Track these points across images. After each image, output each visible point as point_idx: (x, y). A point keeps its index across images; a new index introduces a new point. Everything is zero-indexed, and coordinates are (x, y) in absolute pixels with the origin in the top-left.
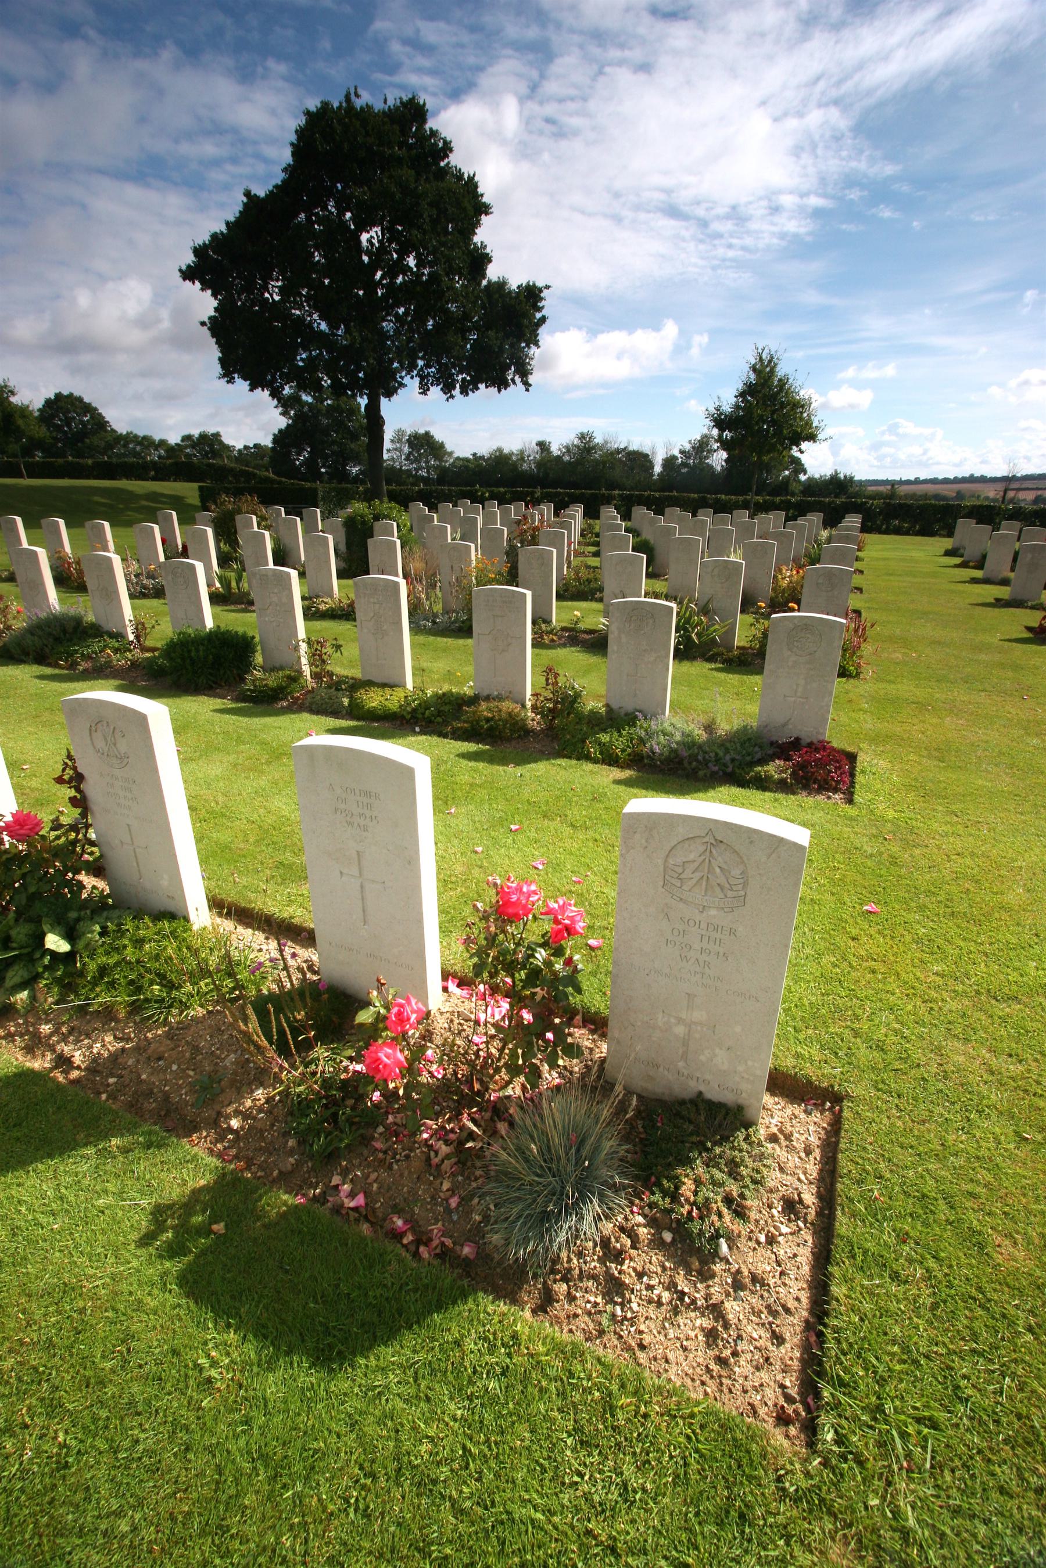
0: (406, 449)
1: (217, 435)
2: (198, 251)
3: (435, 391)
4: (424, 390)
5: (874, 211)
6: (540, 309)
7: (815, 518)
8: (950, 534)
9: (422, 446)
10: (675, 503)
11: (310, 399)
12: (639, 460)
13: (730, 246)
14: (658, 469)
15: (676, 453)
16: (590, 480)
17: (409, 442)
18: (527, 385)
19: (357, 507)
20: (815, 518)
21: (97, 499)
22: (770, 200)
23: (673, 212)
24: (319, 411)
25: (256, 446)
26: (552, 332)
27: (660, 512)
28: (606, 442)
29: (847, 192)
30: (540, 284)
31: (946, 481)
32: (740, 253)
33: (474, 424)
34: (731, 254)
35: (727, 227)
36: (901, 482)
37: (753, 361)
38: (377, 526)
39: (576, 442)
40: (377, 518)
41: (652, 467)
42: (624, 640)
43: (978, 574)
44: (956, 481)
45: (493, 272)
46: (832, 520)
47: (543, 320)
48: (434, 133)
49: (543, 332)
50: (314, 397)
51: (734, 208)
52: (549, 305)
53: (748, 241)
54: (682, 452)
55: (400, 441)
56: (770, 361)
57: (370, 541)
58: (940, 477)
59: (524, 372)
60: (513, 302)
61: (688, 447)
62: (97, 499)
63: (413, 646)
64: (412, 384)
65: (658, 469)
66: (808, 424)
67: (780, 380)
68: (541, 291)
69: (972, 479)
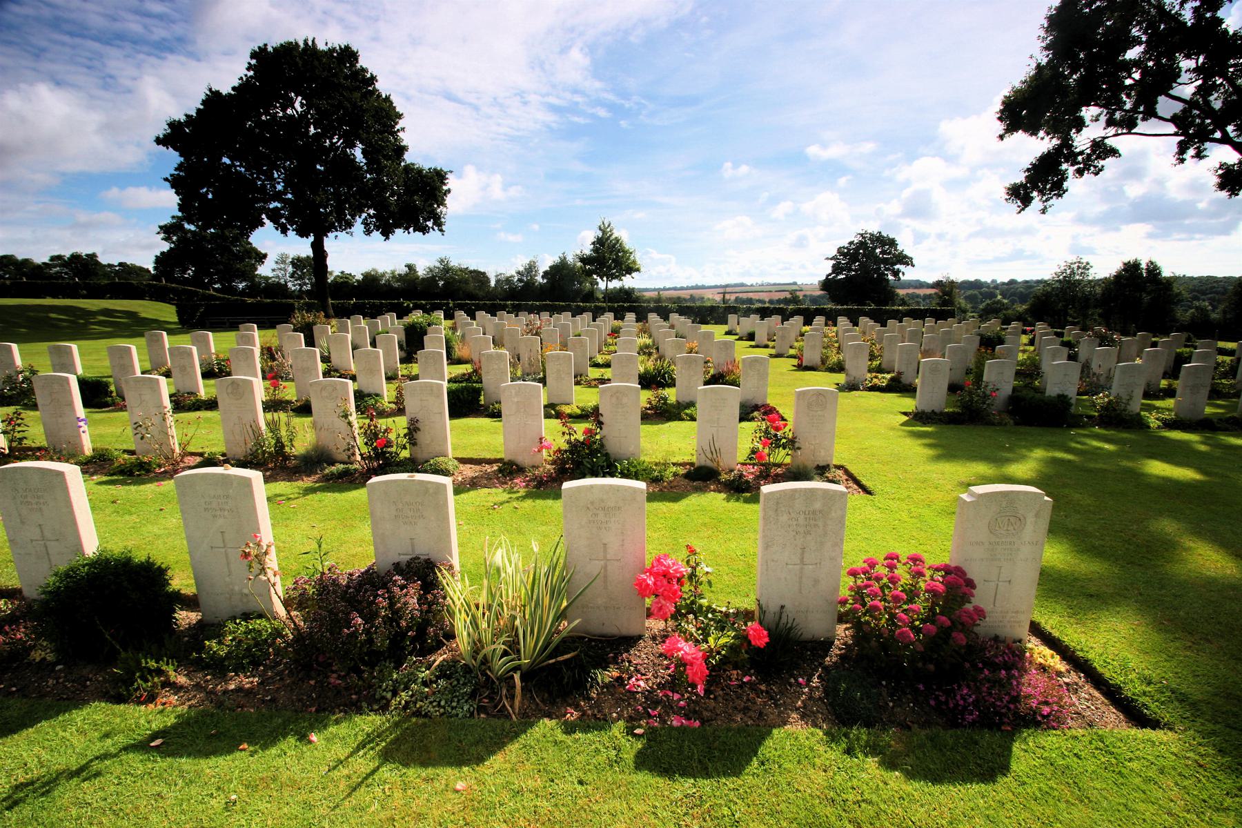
0: (290, 269)
1: (92, 257)
2: (172, 125)
3: (376, 235)
4: (368, 232)
7: (798, 319)
8: (726, 323)
9: (305, 267)
10: (503, 308)
11: (192, 228)
12: (480, 277)
14: (493, 283)
16: (457, 292)
17: (292, 263)
18: (441, 230)
19: (417, 316)
20: (798, 319)
21: (53, 315)
23: (450, 97)
24: (205, 237)
25: (121, 264)
27: (494, 315)
31: (682, 289)
33: (356, 253)
34: (502, 130)
36: (664, 289)
38: (429, 329)
39: (438, 265)
40: (429, 325)
43: (753, 343)
44: (688, 288)
45: (409, 158)
46: (619, 316)
47: (449, 191)
48: (364, 70)
50: (197, 226)
54: (519, 273)
55: (284, 262)
57: (425, 338)
59: (439, 223)
61: (521, 269)
62: (53, 315)
64: (358, 227)
65: (493, 283)
66: (634, 262)
69: (697, 287)
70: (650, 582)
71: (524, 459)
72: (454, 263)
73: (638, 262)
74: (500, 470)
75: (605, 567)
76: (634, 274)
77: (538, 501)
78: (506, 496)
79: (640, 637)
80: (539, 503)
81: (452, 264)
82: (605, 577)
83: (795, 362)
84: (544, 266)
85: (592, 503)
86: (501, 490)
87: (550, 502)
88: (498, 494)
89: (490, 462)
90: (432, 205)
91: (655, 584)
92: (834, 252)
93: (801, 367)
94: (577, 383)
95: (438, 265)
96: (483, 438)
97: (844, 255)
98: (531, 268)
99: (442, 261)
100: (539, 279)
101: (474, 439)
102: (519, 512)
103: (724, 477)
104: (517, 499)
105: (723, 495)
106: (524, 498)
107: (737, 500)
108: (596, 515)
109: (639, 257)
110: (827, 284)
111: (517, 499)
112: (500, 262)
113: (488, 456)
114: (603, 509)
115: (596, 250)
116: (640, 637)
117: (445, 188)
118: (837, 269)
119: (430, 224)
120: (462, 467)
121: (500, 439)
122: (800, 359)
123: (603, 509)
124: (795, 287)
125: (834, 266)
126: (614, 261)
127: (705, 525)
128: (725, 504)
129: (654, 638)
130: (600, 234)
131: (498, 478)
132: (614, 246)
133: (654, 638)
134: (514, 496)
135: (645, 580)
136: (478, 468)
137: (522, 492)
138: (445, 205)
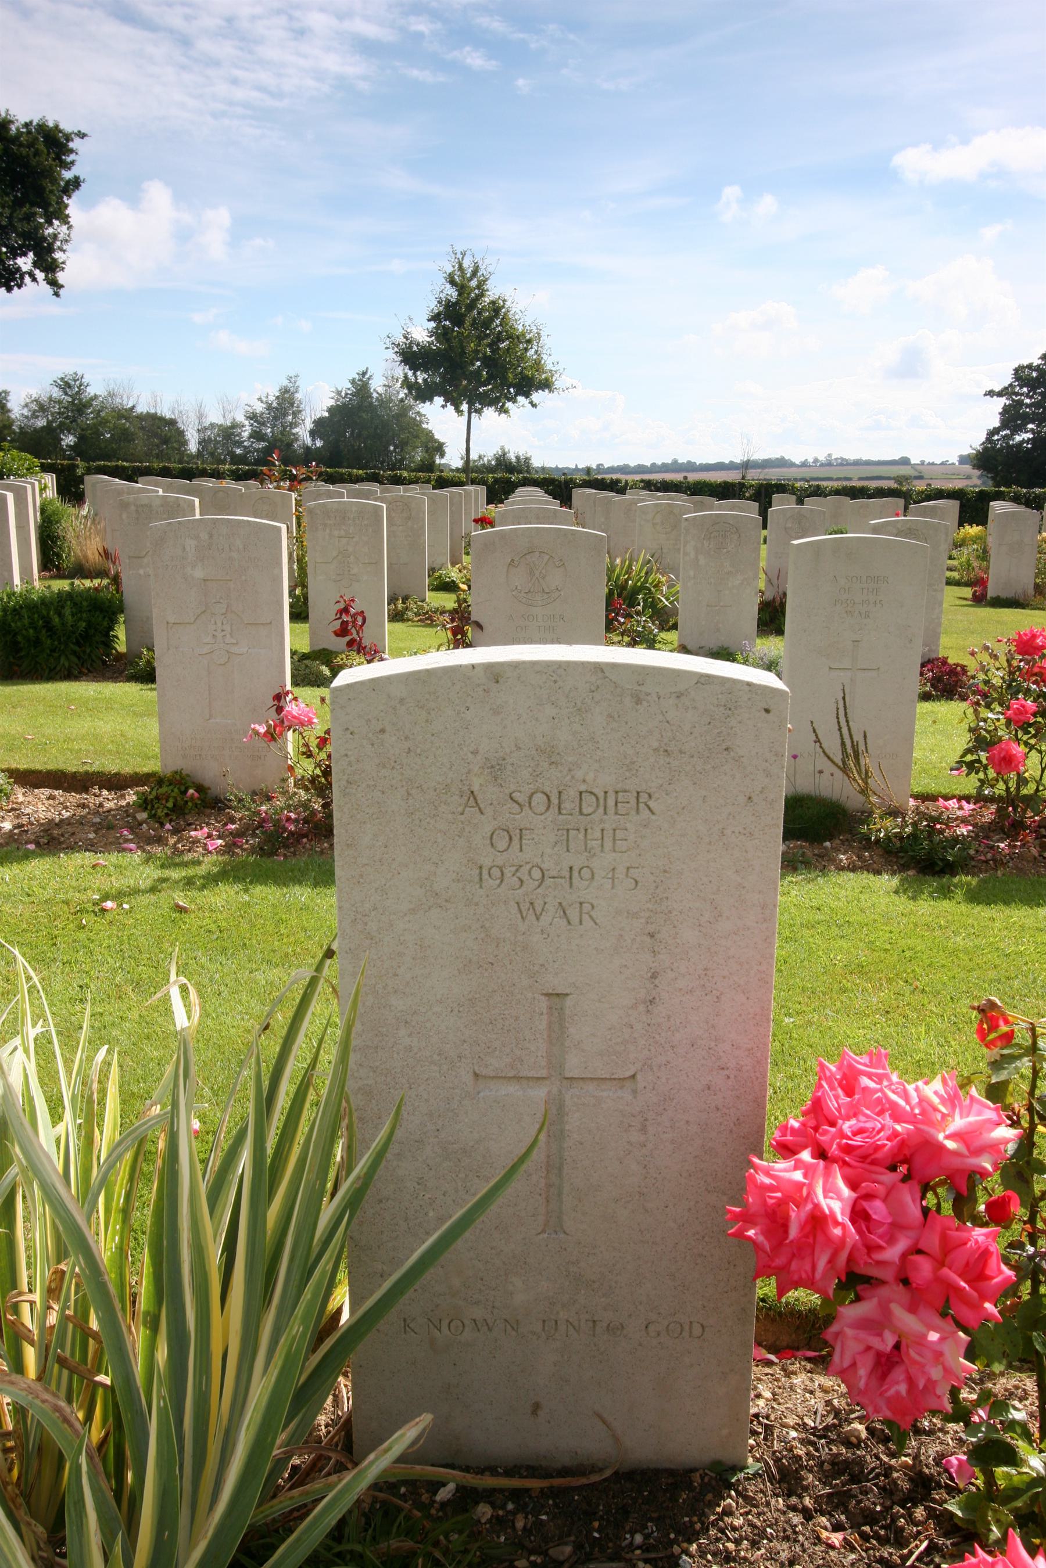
5: (456, 54)
6: (68, 166)
13: (235, 82)
14: (193, 447)
15: (240, 418)
18: (53, 283)
22: (291, 18)
26: (89, 205)
28: (111, 395)
29: (412, 19)
30: (67, 126)
32: (255, 94)
34: (240, 94)
35: (226, 50)
37: (449, 270)
39: (56, 393)
41: (185, 443)
42: (702, 561)
47: (76, 183)
49: (74, 206)
51: (230, 20)
52: (84, 160)
53: (265, 77)
54: (253, 417)
56: (475, 273)
58: (633, 464)
60: (24, 151)
63: (292, 631)
65: (193, 447)
66: (538, 365)
67: (493, 303)
68: (68, 138)
70: (835, 1199)
71: (224, 771)
72: (96, 388)
73: (548, 363)
74: (145, 803)
75: (553, 1120)
76: (537, 396)
77: (259, 890)
78: (151, 873)
79: (721, 1477)
80: (266, 896)
81: (91, 391)
82: (555, 1166)
83: (968, 592)
84: (318, 400)
85: (496, 769)
86: (137, 856)
87: (301, 894)
88: (131, 867)
89: (116, 783)
90: (29, 217)
91: (858, 1214)
92: (1006, 379)
93: (979, 600)
94: (397, 617)
95: (56, 393)
96: (107, 726)
97: (1032, 384)
98: (285, 405)
99: (65, 385)
100: (303, 433)
101: (83, 725)
102: (191, 921)
103: (883, 827)
104: (189, 882)
105: (888, 881)
106: (212, 880)
107: (945, 893)
108: (515, 835)
109: (554, 353)
110: (989, 458)
111: (189, 882)
112: (204, 387)
113: (112, 766)
114: (555, 802)
115: (441, 334)
116: (721, 1477)
117: (67, 175)
118: (1012, 418)
119: (25, 263)
120: (20, 794)
121: (151, 730)
122: (982, 582)
123: (555, 802)
124: (904, 471)
125: (1006, 410)
126: (487, 361)
127: (861, 970)
128: (902, 903)
129: (787, 1478)
130: (452, 293)
131: (134, 827)
132: (487, 323)
133: (787, 1478)
134: (175, 874)
135: (797, 1194)
136: (74, 798)
137: (209, 864)
138: (65, 220)
